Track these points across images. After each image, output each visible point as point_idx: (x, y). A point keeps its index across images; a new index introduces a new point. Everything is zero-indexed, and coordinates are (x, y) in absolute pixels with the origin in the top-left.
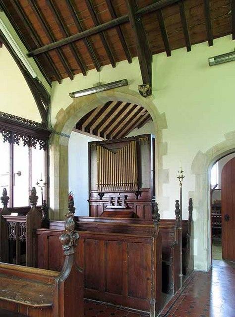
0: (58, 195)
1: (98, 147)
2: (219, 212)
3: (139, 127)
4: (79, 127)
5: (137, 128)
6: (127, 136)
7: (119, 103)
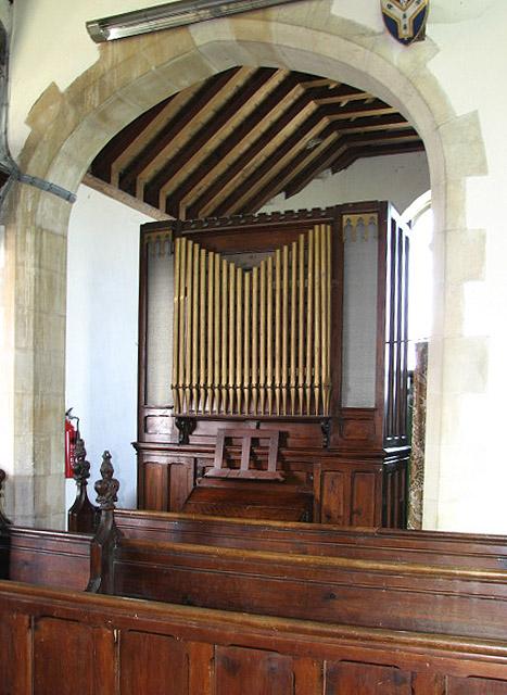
0: (28, 419)
1: (181, 242)
2: (199, 461)
3: (290, 191)
4: (100, 171)
5: (283, 194)
6: (267, 209)
7: (263, 74)
